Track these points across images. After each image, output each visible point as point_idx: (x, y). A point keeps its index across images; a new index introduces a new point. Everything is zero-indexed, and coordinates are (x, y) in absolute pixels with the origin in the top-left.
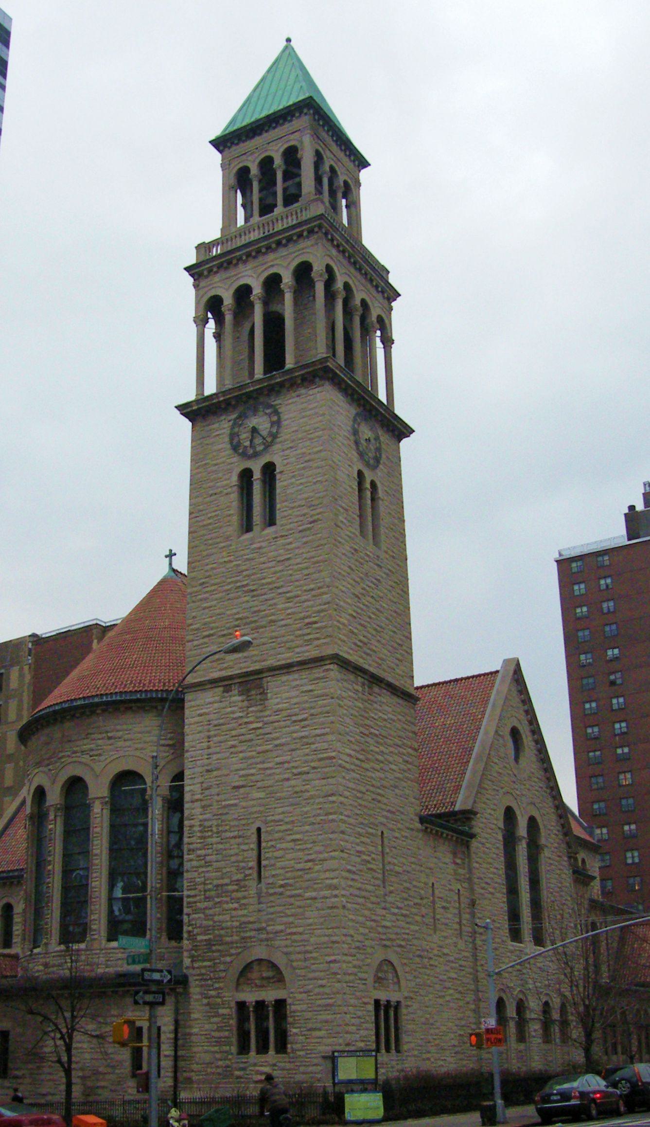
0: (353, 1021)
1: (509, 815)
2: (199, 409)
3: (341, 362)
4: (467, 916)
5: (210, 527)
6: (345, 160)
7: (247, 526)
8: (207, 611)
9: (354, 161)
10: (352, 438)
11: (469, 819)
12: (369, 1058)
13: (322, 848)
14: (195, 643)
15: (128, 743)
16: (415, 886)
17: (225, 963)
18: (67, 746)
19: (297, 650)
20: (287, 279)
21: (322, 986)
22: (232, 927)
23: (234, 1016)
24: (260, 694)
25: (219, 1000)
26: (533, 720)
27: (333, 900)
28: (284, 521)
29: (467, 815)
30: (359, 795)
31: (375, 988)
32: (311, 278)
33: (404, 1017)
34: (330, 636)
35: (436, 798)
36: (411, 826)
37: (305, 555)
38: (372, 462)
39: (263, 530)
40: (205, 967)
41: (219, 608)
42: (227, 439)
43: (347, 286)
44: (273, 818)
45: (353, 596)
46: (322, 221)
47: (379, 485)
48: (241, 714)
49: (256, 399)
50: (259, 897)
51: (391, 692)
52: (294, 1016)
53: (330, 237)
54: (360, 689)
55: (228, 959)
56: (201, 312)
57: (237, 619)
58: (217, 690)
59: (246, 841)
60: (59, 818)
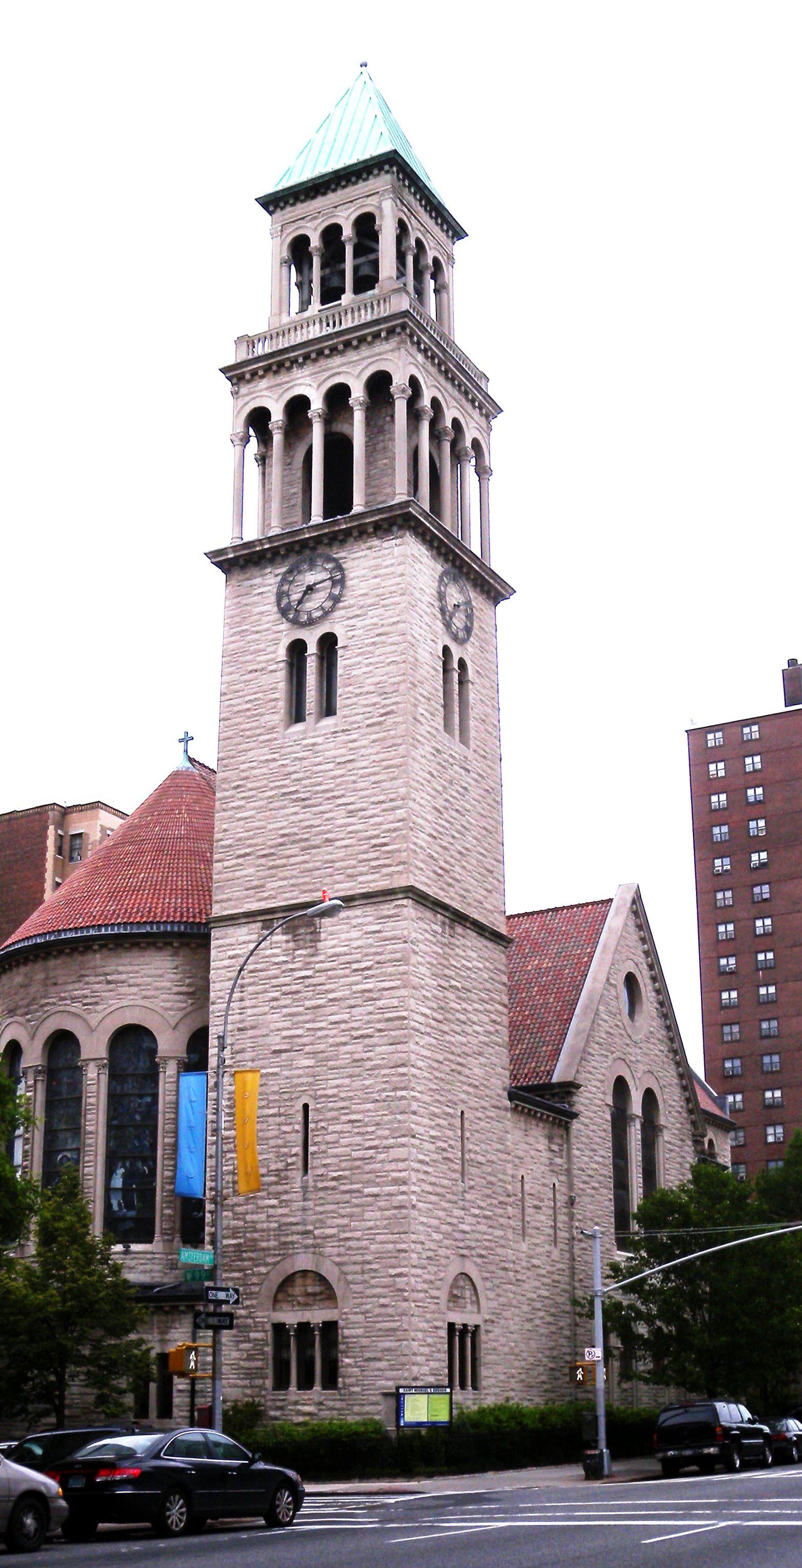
0: (422, 1350)
1: (621, 1087)
2: (236, 558)
3: (426, 507)
4: (565, 1218)
5: (248, 713)
6: (436, 230)
7: (297, 714)
8: (242, 822)
9: (447, 232)
10: (437, 604)
11: (570, 1094)
12: (441, 1396)
13: (387, 1133)
14: (226, 864)
15: (134, 990)
16: (500, 1180)
17: (260, 1274)
18: (52, 989)
19: (361, 879)
20: (358, 393)
21: (383, 1306)
22: (269, 1230)
23: (270, 1340)
24: (311, 933)
25: (250, 1321)
26: (654, 965)
27: (400, 1197)
28: (346, 712)
29: (569, 1089)
30: (435, 1065)
31: (449, 1309)
32: (389, 392)
33: (483, 1346)
34: (404, 863)
35: (528, 1066)
36: (499, 1104)
37: (373, 758)
38: (461, 634)
39: (318, 721)
40: (232, 1279)
41: (260, 820)
42: (273, 599)
43: (435, 403)
44: (326, 1092)
45: (433, 811)
46: (406, 320)
47: (469, 664)
48: (285, 959)
49: (313, 549)
50: (305, 1192)
51: (477, 933)
52: (347, 1343)
53: (415, 339)
54: (440, 930)
55: (263, 1270)
56: (240, 429)
57: (283, 836)
58: (253, 926)
59: (289, 1121)
60: (39, 1085)
